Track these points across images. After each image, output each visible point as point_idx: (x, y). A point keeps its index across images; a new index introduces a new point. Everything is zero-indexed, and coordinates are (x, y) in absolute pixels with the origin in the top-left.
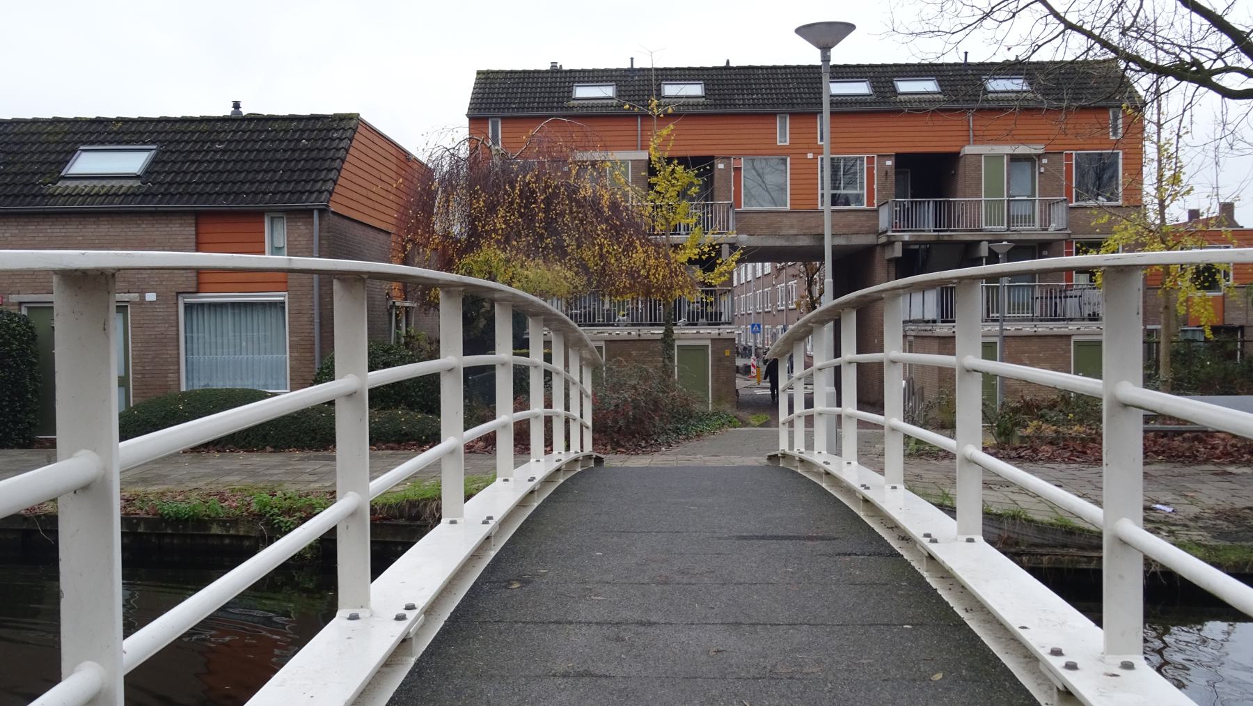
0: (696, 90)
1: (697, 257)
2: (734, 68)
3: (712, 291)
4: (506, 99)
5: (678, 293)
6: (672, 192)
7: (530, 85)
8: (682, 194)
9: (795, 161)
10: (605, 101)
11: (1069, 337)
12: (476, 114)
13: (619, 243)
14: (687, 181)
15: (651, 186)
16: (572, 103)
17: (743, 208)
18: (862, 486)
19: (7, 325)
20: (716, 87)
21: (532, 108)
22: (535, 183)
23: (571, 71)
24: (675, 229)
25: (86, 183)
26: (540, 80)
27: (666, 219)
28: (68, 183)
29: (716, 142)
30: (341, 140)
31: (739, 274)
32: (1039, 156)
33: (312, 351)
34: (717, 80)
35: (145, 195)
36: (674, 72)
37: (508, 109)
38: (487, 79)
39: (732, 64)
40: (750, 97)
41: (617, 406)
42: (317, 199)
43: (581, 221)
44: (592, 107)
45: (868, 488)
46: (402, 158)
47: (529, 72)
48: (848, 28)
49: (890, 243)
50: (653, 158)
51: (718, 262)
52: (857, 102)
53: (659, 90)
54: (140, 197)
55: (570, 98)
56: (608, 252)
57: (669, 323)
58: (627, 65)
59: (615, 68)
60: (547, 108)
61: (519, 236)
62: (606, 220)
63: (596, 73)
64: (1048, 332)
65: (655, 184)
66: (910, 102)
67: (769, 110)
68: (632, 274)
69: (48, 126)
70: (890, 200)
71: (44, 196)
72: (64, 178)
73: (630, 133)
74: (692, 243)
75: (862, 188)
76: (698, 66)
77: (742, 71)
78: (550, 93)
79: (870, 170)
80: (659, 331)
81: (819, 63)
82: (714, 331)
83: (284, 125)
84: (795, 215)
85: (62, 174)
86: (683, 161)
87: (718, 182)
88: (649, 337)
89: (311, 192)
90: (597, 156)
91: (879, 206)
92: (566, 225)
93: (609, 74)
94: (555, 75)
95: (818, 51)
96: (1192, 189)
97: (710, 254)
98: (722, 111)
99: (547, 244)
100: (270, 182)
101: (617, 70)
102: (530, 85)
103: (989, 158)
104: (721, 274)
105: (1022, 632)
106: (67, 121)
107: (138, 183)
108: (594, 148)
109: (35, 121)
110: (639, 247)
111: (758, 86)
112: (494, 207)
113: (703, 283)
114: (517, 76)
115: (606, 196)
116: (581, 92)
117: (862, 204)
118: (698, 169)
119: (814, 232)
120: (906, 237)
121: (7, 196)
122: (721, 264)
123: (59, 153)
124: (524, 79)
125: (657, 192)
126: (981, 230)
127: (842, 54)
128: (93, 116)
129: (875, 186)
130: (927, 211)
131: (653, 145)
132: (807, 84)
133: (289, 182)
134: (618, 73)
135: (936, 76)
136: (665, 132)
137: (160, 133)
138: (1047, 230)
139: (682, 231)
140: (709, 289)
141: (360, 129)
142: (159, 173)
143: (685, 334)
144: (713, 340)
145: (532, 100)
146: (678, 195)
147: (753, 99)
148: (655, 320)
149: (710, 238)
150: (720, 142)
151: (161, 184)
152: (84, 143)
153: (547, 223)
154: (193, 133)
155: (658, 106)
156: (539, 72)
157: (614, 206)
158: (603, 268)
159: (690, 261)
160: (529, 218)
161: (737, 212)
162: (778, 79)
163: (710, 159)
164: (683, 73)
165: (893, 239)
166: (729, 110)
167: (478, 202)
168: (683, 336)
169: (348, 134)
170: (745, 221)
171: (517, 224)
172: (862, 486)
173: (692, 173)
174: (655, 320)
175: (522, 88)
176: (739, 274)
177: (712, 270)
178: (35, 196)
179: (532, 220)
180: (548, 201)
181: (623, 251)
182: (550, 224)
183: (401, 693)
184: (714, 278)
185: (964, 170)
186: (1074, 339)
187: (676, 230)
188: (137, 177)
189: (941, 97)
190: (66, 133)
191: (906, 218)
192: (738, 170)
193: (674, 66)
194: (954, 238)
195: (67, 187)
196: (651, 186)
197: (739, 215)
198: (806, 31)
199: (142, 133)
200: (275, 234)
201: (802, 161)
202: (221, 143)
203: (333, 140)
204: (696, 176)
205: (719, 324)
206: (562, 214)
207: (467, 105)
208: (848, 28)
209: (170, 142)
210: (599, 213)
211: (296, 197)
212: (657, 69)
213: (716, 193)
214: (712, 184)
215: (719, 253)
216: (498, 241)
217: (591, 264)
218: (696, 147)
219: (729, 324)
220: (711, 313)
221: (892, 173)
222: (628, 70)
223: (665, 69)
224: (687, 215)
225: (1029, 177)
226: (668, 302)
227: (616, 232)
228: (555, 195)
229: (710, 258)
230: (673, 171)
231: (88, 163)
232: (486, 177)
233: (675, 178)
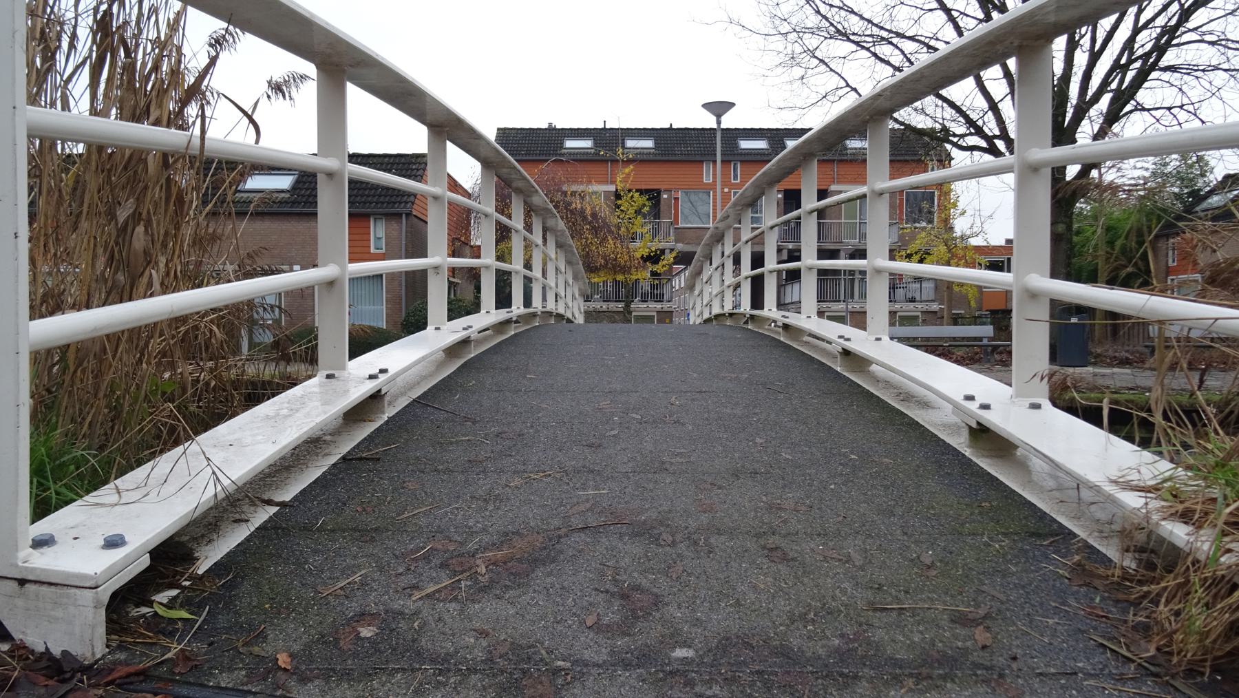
0: (648, 143)
2: (674, 129)
6: (632, 211)
8: (638, 212)
13: (597, 238)
14: (641, 203)
15: (618, 207)
16: (563, 151)
17: (680, 226)
18: (840, 337)
23: (562, 129)
24: (633, 239)
28: (243, 195)
30: (418, 170)
31: (680, 281)
33: (400, 303)
35: (293, 203)
38: (504, 133)
39: (674, 127)
42: (405, 207)
43: (573, 224)
45: (848, 340)
46: (452, 184)
48: (731, 105)
50: (619, 188)
52: (761, 155)
53: (623, 143)
55: (562, 147)
56: (591, 243)
58: (601, 126)
62: (590, 223)
63: (580, 131)
67: (698, 158)
73: (603, 172)
80: (621, 305)
81: (715, 126)
82: (659, 306)
83: (380, 160)
86: (641, 192)
87: (663, 207)
88: (615, 309)
89: (400, 203)
90: (580, 188)
95: (714, 118)
96: (965, 212)
100: (374, 196)
104: (663, 266)
107: (288, 195)
108: (582, 183)
116: (570, 144)
125: (621, 210)
126: (841, 242)
127: (730, 121)
131: (618, 179)
133: (386, 196)
136: (627, 170)
142: (301, 189)
146: (636, 212)
151: (303, 196)
155: (623, 154)
157: (594, 215)
163: (659, 192)
166: (671, 158)
169: (423, 166)
170: (681, 234)
172: (840, 337)
173: (645, 198)
176: (680, 281)
177: (658, 263)
183: (459, 532)
186: (898, 314)
192: (677, 199)
195: (242, 197)
196: (618, 207)
198: (708, 106)
200: (377, 229)
203: (412, 170)
204: (648, 200)
208: (731, 105)
210: (585, 218)
211: (391, 205)
212: (622, 129)
222: (602, 129)
223: (628, 129)
224: (642, 227)
227: (596, 231)
229: (656, 254)
230: (632, 197)
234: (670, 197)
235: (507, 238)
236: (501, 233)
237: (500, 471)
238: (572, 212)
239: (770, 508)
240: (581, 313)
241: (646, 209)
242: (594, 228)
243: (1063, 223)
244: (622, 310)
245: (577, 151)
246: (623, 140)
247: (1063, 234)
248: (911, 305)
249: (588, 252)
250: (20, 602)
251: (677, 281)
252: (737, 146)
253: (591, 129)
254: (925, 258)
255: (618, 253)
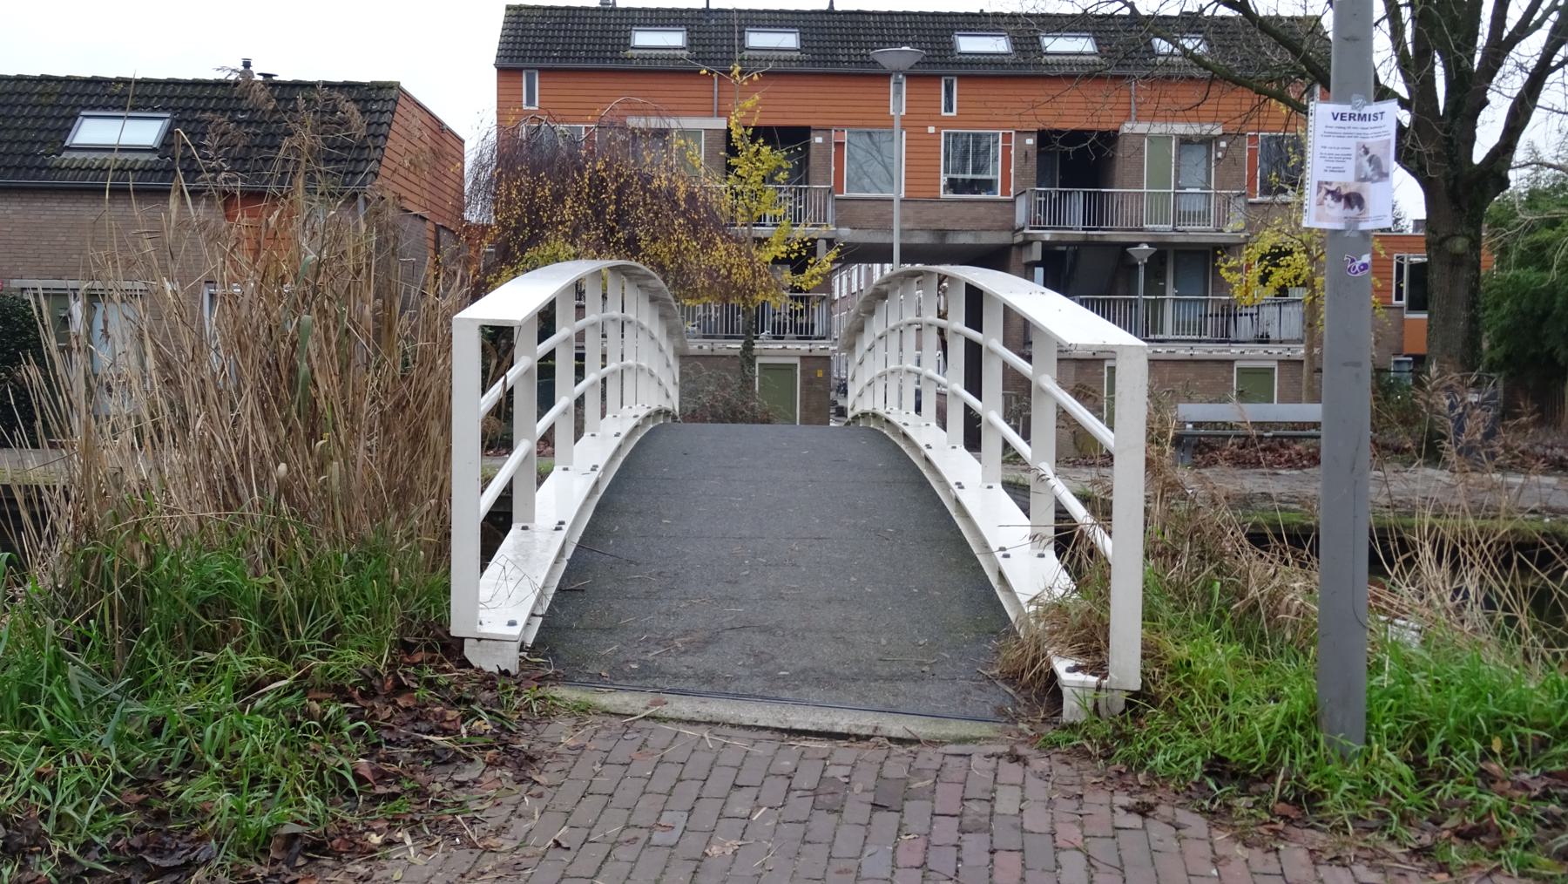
0: (789, 40)
1: (785, 256)
3: (802, 298)
4: (545, 44)
5: (760, 298)
6: (756, 177)
7: (576, 27)
8: (769, 179)
9: (911, 136)
10: (672, 52)
11: (1231, 362)
12: (507, 64)
13: (697, 239)
14: (774, 164)
16: (630, 53)
17: (845, 195)
19: (23, 313)
20: (815, 38)
21: (580, 58)
22: (605, 170)
23: (628, 10)
24: (760, 220)
25: (95, 155)
26: (588, 21)
27: (749, 210)
28: (74, 155)
29: (811, 109)
30: (382, 113)
31: (849, 280)
32: (1217, 138)
34: (818, 48)
36: (761, 16)
37: (548, 58)
38: (519, 16)
40: (858, 51)
41: (694, 411)
43: (656, 214)
44: (656, 59)
46: (435, 128)
47: (575, 9)
49: (1027, 243)
51: (811, 261)
52: (992, 63)
53: (742, 39)
54: (160, 174)
55: (627, 46)
56: (686, 249)
57: (750, 336)
59: (685, 7)
60: (598, 58)
61: (587, 228)
62: (684, 214)
64: (1205, 355)
65: (735, 167)
66: (1058, 65)
68: (711, 273)
69: (36, 85)
70: (1028, 189)
71: (50, 169)
72: (69, 149)
74: (779, 238)
75: (995, 173)
76: (792, 8)
77: (848, 17)
78: (601, 38)
79: (1006, 150)
80: (737, 345)
82: (804, 347)
84: (911, 204)
85: (67, 144)
87: (815, 160)
88: (724, 352)
91: (1016, 196)
92: (639, 218)
93: (678, 15)
94: (607, 14)
97: (800, 253)
98: (822, 69)
99: (619, 239)
101: (688, 10)
102: (576, 27)
103: (1154, 139)
104: (813, 277)
105: (905, 428)
106: (58, 80)
107: (155, 157)
109: (20, 79)
110: (720, 244)
111: (868, 38)
112: (561, 196)
113: (794, 289)
114: (558, 13)
115: (682, 189)
116: (643, 39)
117: (995, 193)
118: (788, 151)
119: (934, 226)
120: (1047, 235)
121: (7, 168)
122: (812, 265)
123: (57, 118)
124: (567, 18)
128: (89, 75)
129: (1012, 171)
130: (1077, 202)
132: (931, 36)
134: (689, 15)
135: (1094, 32)
136: (749, 104)
137: (170, 98)
138: (1222, 231)
139: (768, 222)
140: (797, 293)
141: (402, 100)
143: (769, 349)
144: (803, 358)
145: (579, 47)
147: (862, 55)
148: (733, 332)
149: (801, 232)
150: (818, 109)
152: (84, 108)
153: (618, 215)
154: (209, 99)
156: (587, 9)
157: (691, 198)
158: (681, 266)
159: (776, 261)
160: (599, 214)
161: (837, 199)
162: (894, 29)
164: (772, 16)
165: (1030, 238)
167: (543, 190)
168: (764, 352)
169: (390, 106)
170: (847, 211)
171: (585, 215)
173: (780, 154)
174: (733, 332)
175: (565, 30)
176: (849, 280)
178: (39, 169)
179: (603, 212)
180: (619, 191)
181: (702, 248)
182: (620, 216)
184: (809, 279)
185: (1122, 153)
186: (1237, 364)
187: (760, 221)
188: (153, 150)
189: (1097, 59)
190: (60, 95)
191: (1053, 213)
192: (840, 145)
193: (761, 8)
194: (1107, 239)
195: (74, 159)
197: (840, 203)
199: (150, 98)
201: (920, 136)
202: (244, 112)
204: (785, 158)
205: (810, 338)
206: (635, 206)
207: (495, 52)
209: (185, 110)
210: (676, 203)
212: (740, 11)
213: (812, 174)
214: (807, 164)
215: (813, 252)
216: (565, 234)
217: (667, 262)
218: (788, 115)
219: (824, 338)
220: (801, 325)
221: (1033, 155)
223: (750, 11)
224: (774, 203)
225: (1204, 164)
226: (749, 309)
227: (694, 228)
228: (627, 184)
231: (93, 131)
232: (551, 162)
233: (759, 160)
234: (827, 141)
235: (541, 238)
236: (531, 231)
237: (671, 598)
238: (654, 195)
239: (845, 619)
240: (675, 383)
241: (783, 175)
242: (690, 220)
243: (1464, 235)
244: (737, 353)
245: (655, 52)
246: (742, 32)
247: (1464, 254)
248: (1260, 350)
249: (681, 266)
250: (478, 649)
251: (845, 278)
252: (951, 47)
253: (681, 11)
254: (1271, 272)
255: (732, 265)
